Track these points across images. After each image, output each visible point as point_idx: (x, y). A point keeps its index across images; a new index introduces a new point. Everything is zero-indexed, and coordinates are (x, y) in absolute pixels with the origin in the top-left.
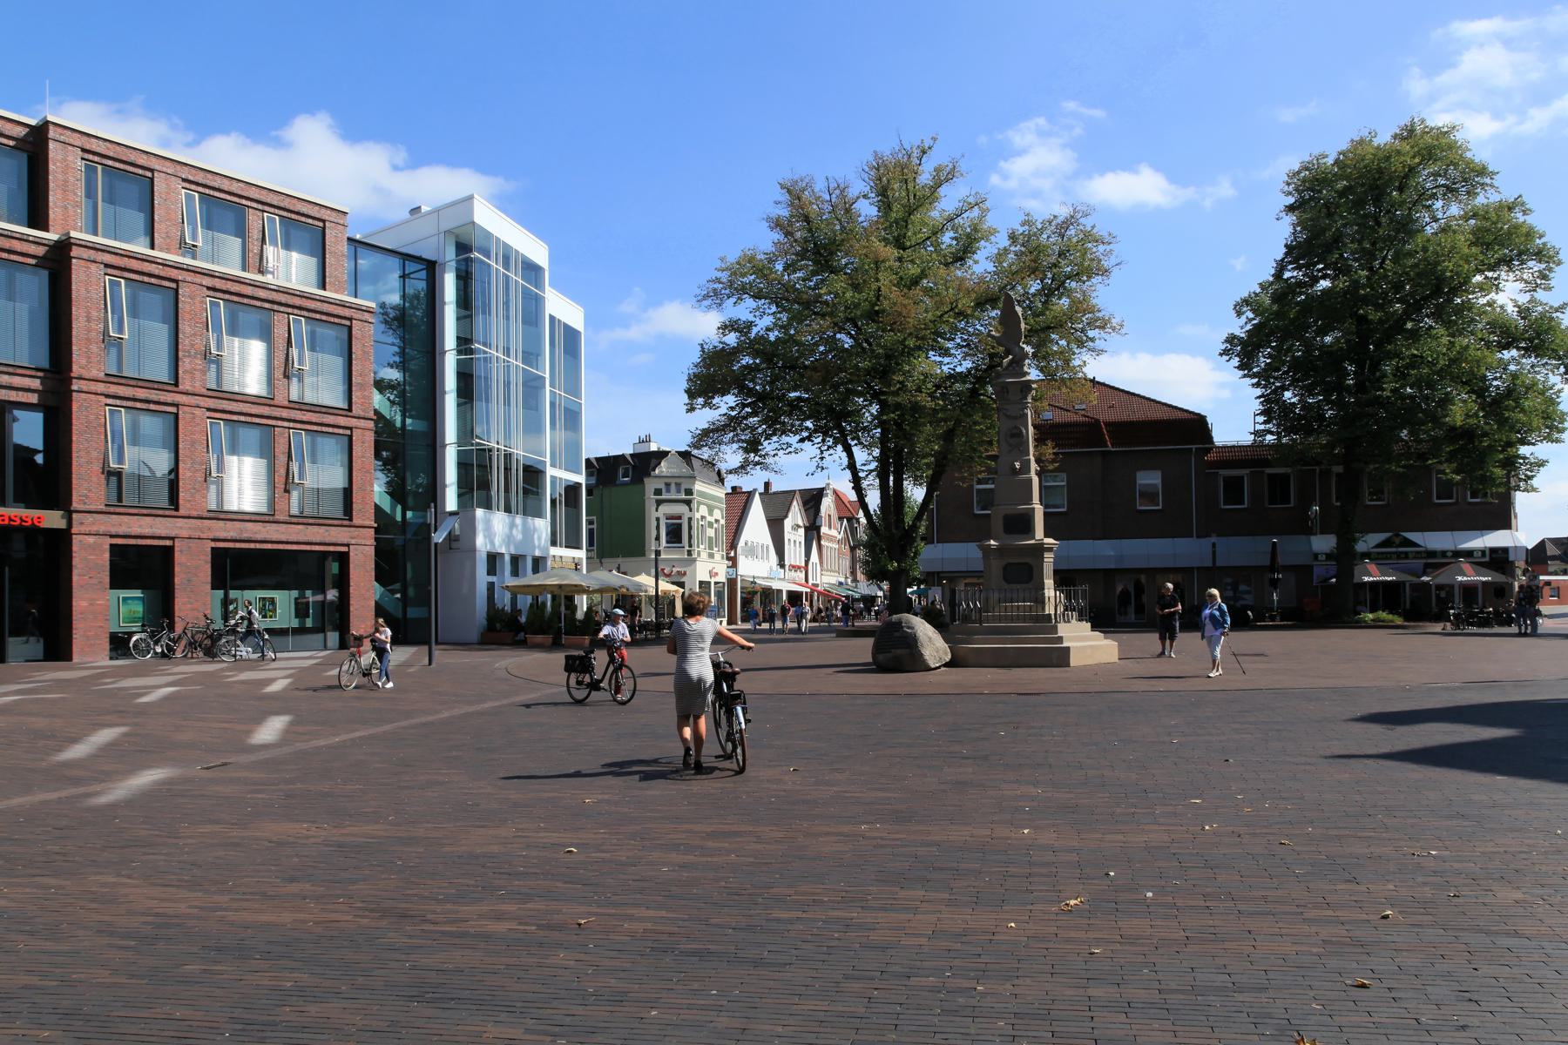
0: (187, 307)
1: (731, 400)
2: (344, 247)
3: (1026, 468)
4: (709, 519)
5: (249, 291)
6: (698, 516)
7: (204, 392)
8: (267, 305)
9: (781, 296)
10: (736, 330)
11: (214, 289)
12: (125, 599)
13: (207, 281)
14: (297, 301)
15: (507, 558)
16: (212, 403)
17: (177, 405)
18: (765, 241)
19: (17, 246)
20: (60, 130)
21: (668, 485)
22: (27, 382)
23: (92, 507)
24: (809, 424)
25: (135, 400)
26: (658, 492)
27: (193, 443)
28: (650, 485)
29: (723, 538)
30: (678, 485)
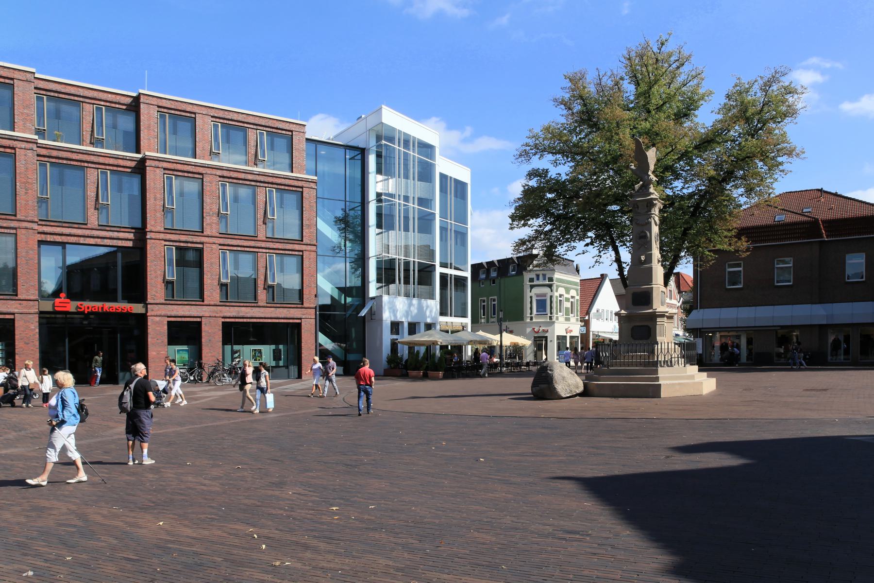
0: (208, 188)
1: (539, 221)
2: (304, 145)
3: (649, 259)
4: (566, 296)
5: (242, 176)
6: (556, 294)
7: (218, 235)
8: (253, 183)
9: (569, 151)
10: (536, 176)
11: (223, 177)
12: (178, 351)
13: (219, 173)
14: (270, 180)
15: (406, 325)
16: (222, 241)
17: (202, 243)
18: (559, 117)
19: (121, 162)
20: (146, 97)
21: (538, 276)
22: (121, 235)
23: (158, 301)
24: (590, 234)
25: (180, 242)
26: (531, 280)
27: (211, 264)
28: (527, 276)
29: (577, 307)
30: (544, 275)
